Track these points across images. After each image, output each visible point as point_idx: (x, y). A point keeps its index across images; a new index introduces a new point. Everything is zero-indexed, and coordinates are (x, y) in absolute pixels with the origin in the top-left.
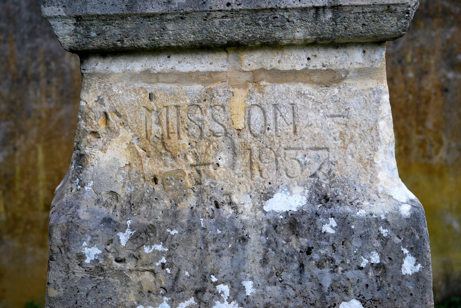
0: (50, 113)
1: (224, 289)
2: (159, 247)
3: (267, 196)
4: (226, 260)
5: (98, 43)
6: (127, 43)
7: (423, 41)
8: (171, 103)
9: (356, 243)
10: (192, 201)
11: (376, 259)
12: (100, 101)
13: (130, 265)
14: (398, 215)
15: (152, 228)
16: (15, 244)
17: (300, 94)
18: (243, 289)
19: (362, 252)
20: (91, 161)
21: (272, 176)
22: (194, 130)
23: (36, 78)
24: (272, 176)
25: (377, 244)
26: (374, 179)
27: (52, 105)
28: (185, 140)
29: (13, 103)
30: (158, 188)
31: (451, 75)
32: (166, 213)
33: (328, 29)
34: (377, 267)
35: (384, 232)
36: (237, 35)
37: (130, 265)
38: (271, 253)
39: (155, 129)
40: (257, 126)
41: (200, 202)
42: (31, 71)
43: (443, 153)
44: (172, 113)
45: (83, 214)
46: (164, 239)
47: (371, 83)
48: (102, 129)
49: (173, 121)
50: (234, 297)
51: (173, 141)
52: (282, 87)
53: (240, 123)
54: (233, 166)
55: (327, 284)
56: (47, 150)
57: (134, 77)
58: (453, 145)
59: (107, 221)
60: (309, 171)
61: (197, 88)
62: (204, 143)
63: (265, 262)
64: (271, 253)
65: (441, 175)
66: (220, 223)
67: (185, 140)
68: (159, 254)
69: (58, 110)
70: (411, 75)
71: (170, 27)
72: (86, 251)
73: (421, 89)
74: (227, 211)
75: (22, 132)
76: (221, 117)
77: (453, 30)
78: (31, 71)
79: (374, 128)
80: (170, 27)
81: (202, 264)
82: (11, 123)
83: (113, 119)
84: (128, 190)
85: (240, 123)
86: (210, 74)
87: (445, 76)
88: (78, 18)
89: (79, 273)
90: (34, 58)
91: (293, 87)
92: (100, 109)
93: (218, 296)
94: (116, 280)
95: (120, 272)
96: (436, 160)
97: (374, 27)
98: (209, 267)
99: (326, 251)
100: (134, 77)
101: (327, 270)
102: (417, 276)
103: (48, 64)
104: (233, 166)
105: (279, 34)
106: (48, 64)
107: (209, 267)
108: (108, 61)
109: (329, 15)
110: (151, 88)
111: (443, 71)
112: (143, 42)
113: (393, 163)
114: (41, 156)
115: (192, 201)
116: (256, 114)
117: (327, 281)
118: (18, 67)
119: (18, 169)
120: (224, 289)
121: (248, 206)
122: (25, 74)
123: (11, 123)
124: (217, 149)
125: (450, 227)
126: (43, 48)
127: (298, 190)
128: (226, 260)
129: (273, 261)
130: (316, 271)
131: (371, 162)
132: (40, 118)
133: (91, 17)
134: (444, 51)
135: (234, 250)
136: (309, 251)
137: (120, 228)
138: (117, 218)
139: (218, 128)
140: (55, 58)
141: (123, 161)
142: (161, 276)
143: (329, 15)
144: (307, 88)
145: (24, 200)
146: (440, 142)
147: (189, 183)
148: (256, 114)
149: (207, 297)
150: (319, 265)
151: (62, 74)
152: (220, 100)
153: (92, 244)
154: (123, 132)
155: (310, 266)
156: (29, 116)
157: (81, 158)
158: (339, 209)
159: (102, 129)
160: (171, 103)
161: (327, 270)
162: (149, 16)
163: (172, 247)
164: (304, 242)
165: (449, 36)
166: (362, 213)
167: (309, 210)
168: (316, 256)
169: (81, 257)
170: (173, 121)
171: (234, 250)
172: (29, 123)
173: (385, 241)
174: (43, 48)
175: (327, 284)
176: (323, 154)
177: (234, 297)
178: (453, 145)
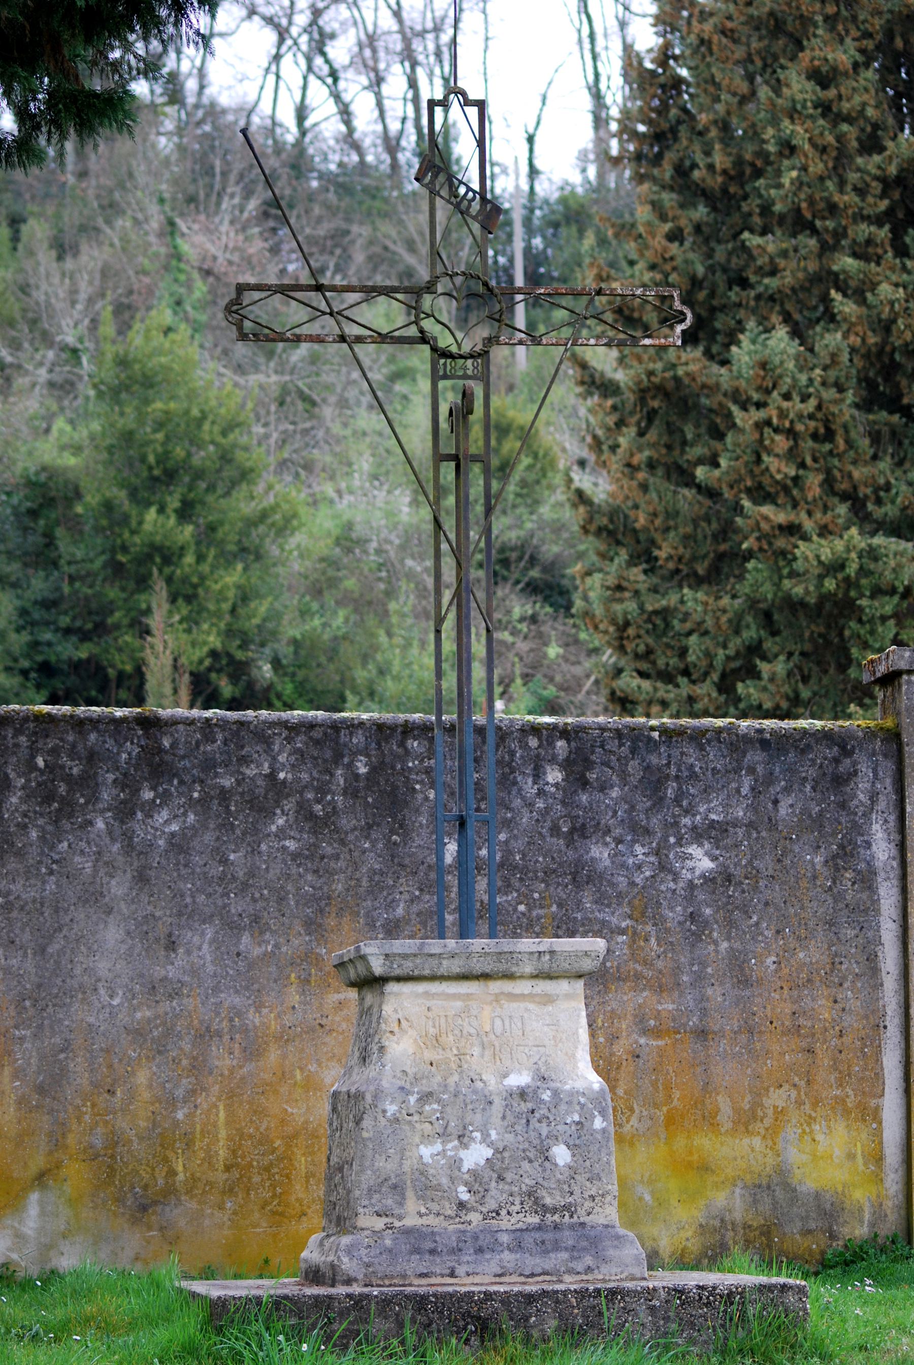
0: (232, 1070)
1: (477, 1135)
2: (435, 1106)
3: (505, 1076)
4: (478, 1116)
5: (397, 972)
6: (416, 973)
7: (614, 1005)
8: (442, 1014)
9: (563, 1107)
10: (456, 1077)
11: (576, 1118)
12: (396, 1011)
13: (416, 1117)
14: (592, 1090)
15: (430, 1094)
16: (193, 1205)
17: (527, 1010)
18: (489, 1135)
19: (567, 1113)
20: (389, 1050)
21: (508, 1063)
22: (457, 1032)
23: (219, 1034)
24: (508, 1063)
25: (578, 1108)
26: (575, 1067)
27: (235, 1062)
28: (451, 1038)
29: (195, 1059)
30: (433, 1069)
31: (642, 1041)
32: (439, 1085)
33: (546, 966)
34: (578, 1123)
35: (582, 1100)
36: (487, 969)
37: (416, 1117)
38: (508, 1113)
39: (432, 1031)
40: (498, 1030)
41: (461, 1078)
42: (215, 1027)
43: (634, 1121)
44: (443, 1020)
45: (385, 1084)
46: (439, 1101)
47: (574, 1004)
48: (396, 1029)
49: (443, 1025)
50: (483, 1141)
51: (443, 1039)
52: (515, 1005)
53: (487, 1028)
54: (482, 1056)
55: (544, 1133)
56: (228, 1107)
57: (417, 995)
58: (645, 1113)
59: (402, 1088)
60: (533, 1060)
61: (459, 1004)
62: (463, 1040)
63: (504, 1118)
64: (508, 1113)
65: (632, 1144)
66: (475, 1092)
67: (451, 1038)
68: (435, 1111)
69: (241, 1067)
70: (602, 1040)
71: (445, 962)
72: (388, 1107)
73: (612, 1054)
74: (479, 1085)
75: (203, 1089)
76: (475, 1023)
77: (645, 994)
78: (215, 1027)
79: (576, 1033)
80: (445, 962)
81: (463, 1118)
82: (193, 1080)
83: (403, 1022)
84: (414, 1070)
85: (487, 1028)
86: (468, 995)
87: (636, 1042)
88: (387, 955)
89: (383, 1122)
90: (218, 1014)
91: (522, 1005)
92: (396, 1016)
93: (473, 1139)
94: (407, 1127)
95: (410, 1122)
96: (627, 1128)
97: (576, 965)
98: (467, 1121)
99: (544, 1111)
100: (417, 995)
101: (544, 1125)
102: (604, 1131)
103: (231, 1020)
104: (482, 1056)
105: (514, 969)
106: (231, 1020)
107: (467, 1121)
108: (401, 984)
109: (547, 957)
110: (429, 1004)
111: (635, 1036)
112: (427, 972)
113: (588, 1058)
114: (222, 1114)
115: (456, 1077)
116: (498, 1022)
117: (544, 1131)
118: (201, 1022)
119: (198, 1127)
120: (477, 1135)
121: (493, 1082)
122: (208, 1029)
123: (193, 1080)
124: (472, 1045)
125: (641, 1199)
126: (226, 1005)
127: (525, 1073)
128: (478, 1116)
129: (510, 1118)
130: (537, 1125)
131: (574, 1056)
132: (222, 1075)
133: (395, 955)
134: (636, 1016)
135: (484, 1110)
136: (533, 1112)
137: (409, 1093)
138: (408, 1086)
139: (473, 1031)
140: (239, 1014)
141: (411, 1051)
142: (436, 1125)
143: (547, 957)
144: (531, 1006)
145: (203, 1159)
146: (632, 1110)
147: (454, 1066)
148: (498, 1022)
149: (466, 1140)
150: (539, 1121)
151: (245, 1030)
152: (474, 1012)
153: (392, 1102)
154: (411, 1032)
155: (534, 1121)
156: (211, 1073)
157: (382, 1049)
158: (552, 1085)
159: (396, 1029)
160: (442, 1014)
161: (544, 1125)
162: (432, 955)
163: (444, 1106)
164: (530, 1105)
165: (641, 1001)
166: (567, 1087)
167: (533, 1085)
168: (537, 1115)
169: (384, 1111)
170: (443, 1025)
171: (484, 1110)
172: (211, 1079)
173: (582, 1106)
174: (226, 1005)
175: (544, 1133)
176: (542, 1049)
177: (483, 1141)
178: (645, 1113)
